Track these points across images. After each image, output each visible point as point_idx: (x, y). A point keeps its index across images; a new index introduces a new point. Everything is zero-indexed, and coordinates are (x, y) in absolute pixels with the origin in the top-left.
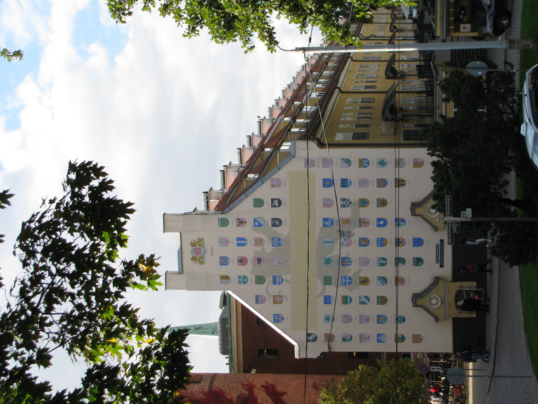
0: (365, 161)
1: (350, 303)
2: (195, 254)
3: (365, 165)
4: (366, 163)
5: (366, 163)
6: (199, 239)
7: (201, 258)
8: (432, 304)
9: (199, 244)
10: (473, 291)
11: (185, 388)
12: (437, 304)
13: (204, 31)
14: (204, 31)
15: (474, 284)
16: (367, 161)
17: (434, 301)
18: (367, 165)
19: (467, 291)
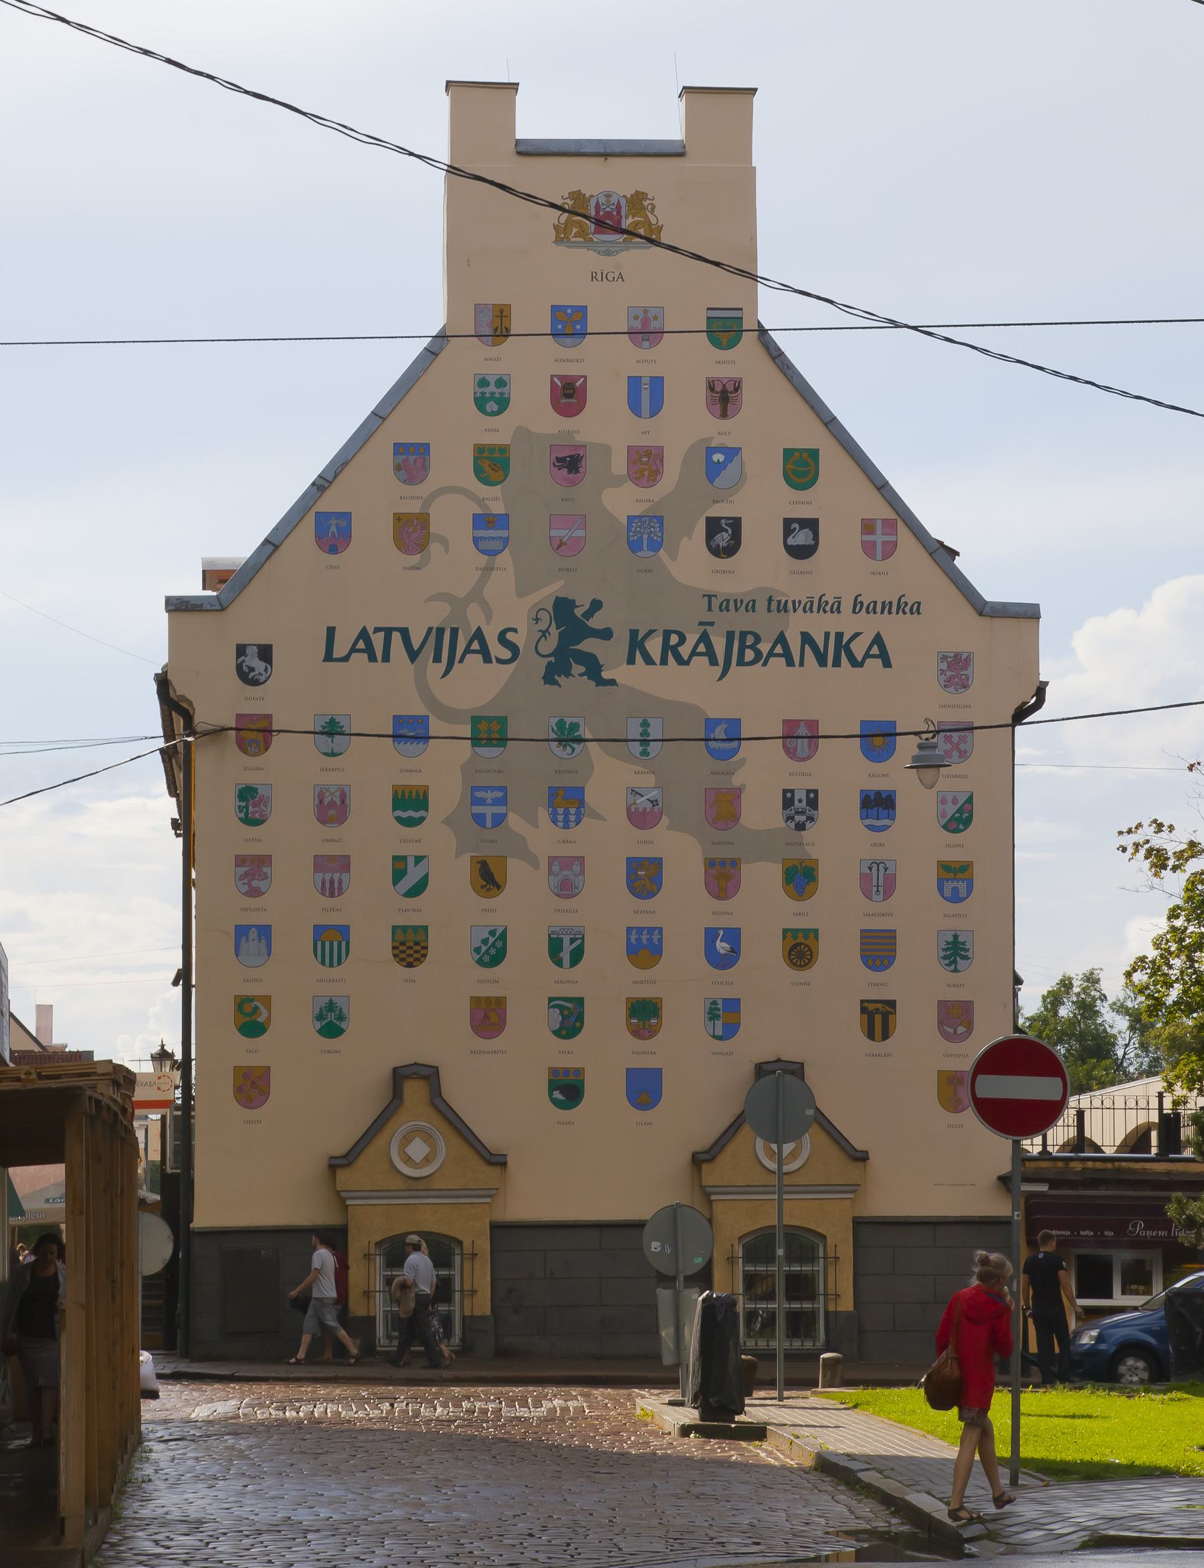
0: (962, 887)
2: (597, 206)
4: (955, 890)
5: (955, 890)
8: (407, 1140)
12: (408, 1160)
17: (418, 1150)
18: (948, 893)
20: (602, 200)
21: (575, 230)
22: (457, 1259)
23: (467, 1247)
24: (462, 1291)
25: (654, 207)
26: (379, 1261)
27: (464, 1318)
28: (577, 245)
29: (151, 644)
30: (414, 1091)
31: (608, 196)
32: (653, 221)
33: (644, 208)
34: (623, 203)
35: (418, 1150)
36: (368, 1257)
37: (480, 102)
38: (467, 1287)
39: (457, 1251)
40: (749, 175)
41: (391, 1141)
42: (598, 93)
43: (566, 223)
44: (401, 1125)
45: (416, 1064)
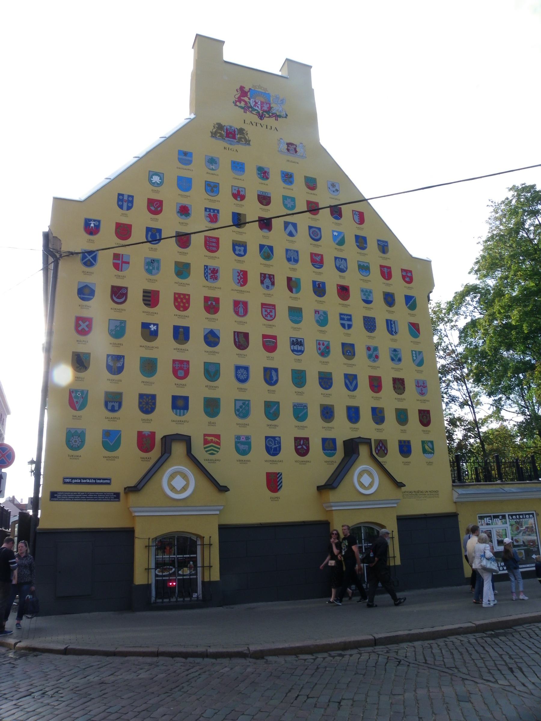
0: (116, 405)
1: (293, 351)
2: (227, 129)
3: (110, 405)
4: (113, 406)
5: (113, 406)
6: (250, 141)
7: (221, 136)
8: (172, 476)
9: (241, 138)
10: (196, 574)
11: (525, 419)
12: (173, 489)
13: (510, 195)
14: (510, 195)
15: (215, 575)
16: (116, 408)
17: (179, 483)
18: (110, 408)
19: (195, 560)
20: (228, 127)
21: (218, 135)
22: (199, 548)
23: (206, 541)
24: (203, 567)
25: (247, 134)
26: (153, 549)
27: (203, 583)
28: (219, 139)
29: (44, 222)
30: (178, 449)
31: (231, 127)
32: (247, 138)
33: (243, 133)
34: (236, 130)
35: (179, 483)
36: (148, 547)
37: (208, 49)
38: (206, 564)
39: (199, 542)
40: (312, 91)
41: (164, 478)
42: (255, 51)
43: (215, 132)
44: (169, 470)
45: (177, 434)
